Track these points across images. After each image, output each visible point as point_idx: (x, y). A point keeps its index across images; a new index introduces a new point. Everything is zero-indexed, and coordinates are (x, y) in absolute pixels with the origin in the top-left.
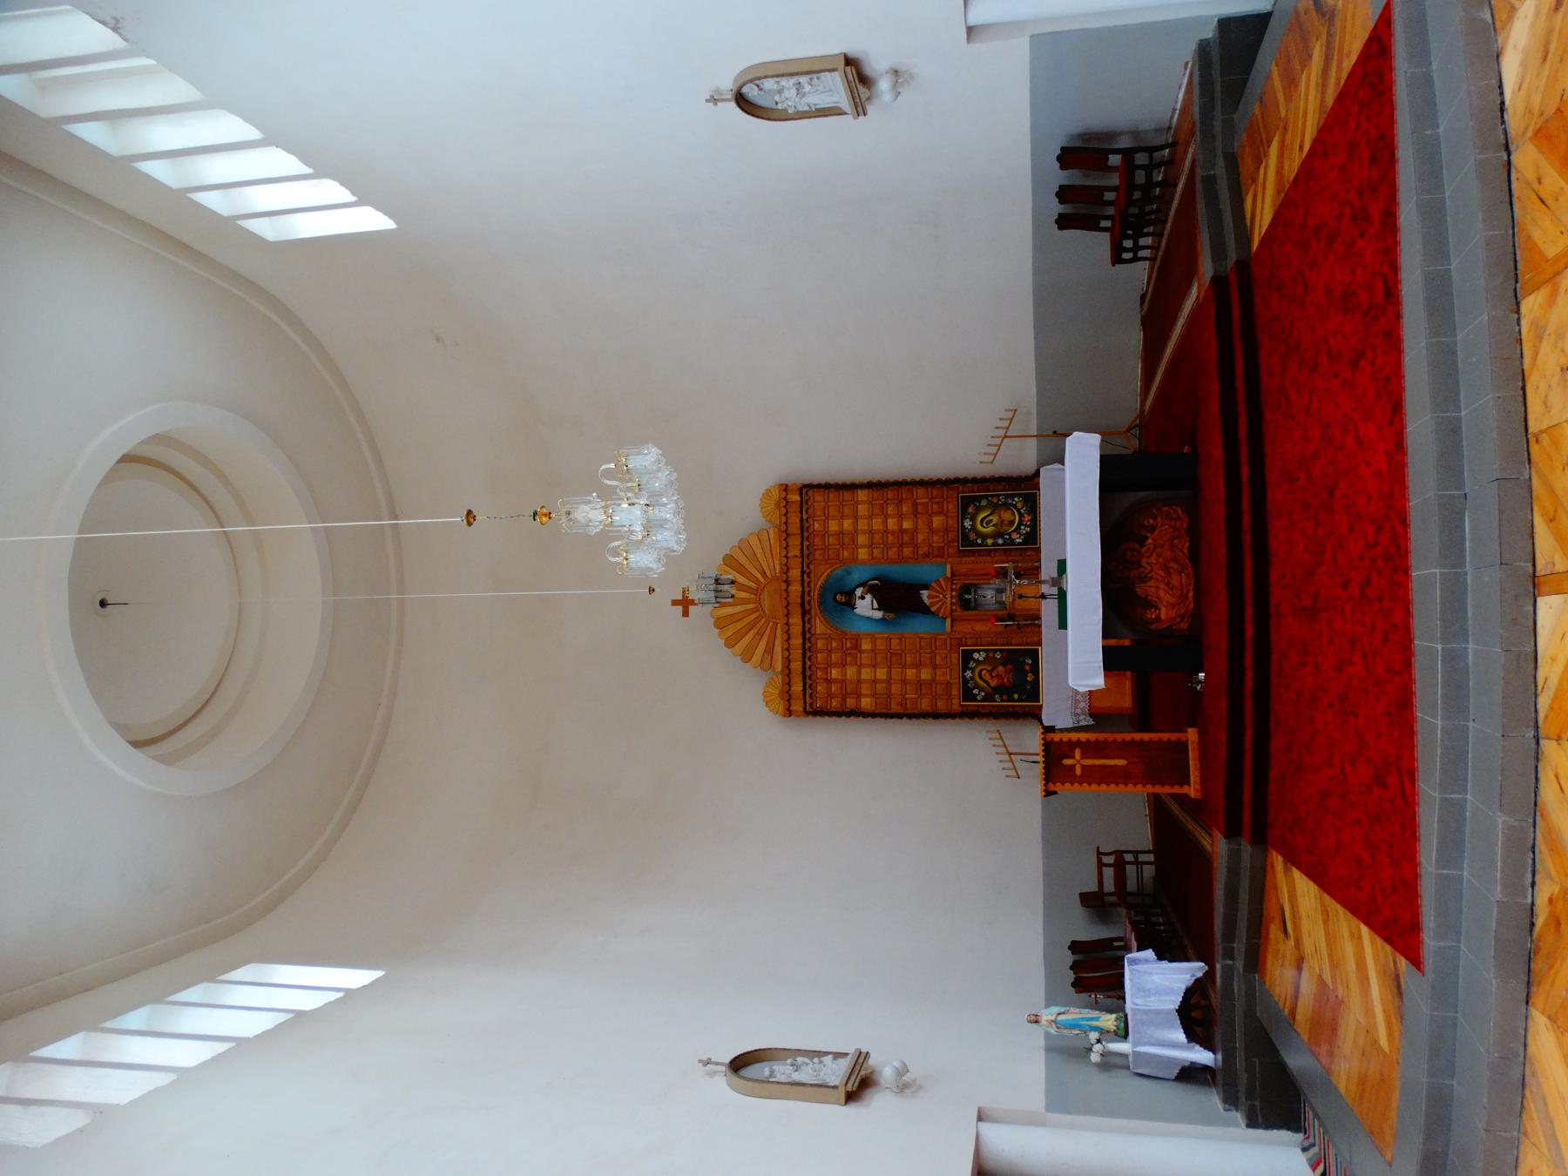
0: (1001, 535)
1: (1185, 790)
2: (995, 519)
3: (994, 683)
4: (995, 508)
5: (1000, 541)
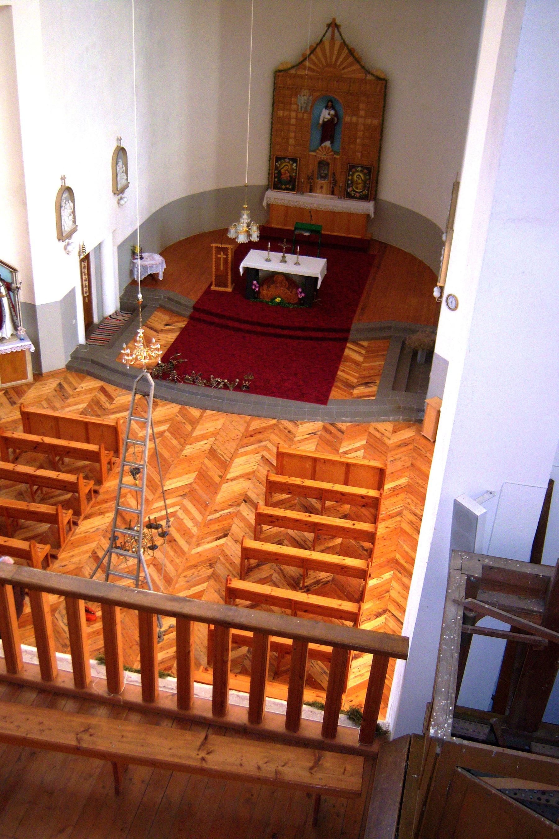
0: (352, 183)
1: (213, 285)
2: (360, 181)
3: (283, 171)
4: (364, 182)
5: (349, 182)
